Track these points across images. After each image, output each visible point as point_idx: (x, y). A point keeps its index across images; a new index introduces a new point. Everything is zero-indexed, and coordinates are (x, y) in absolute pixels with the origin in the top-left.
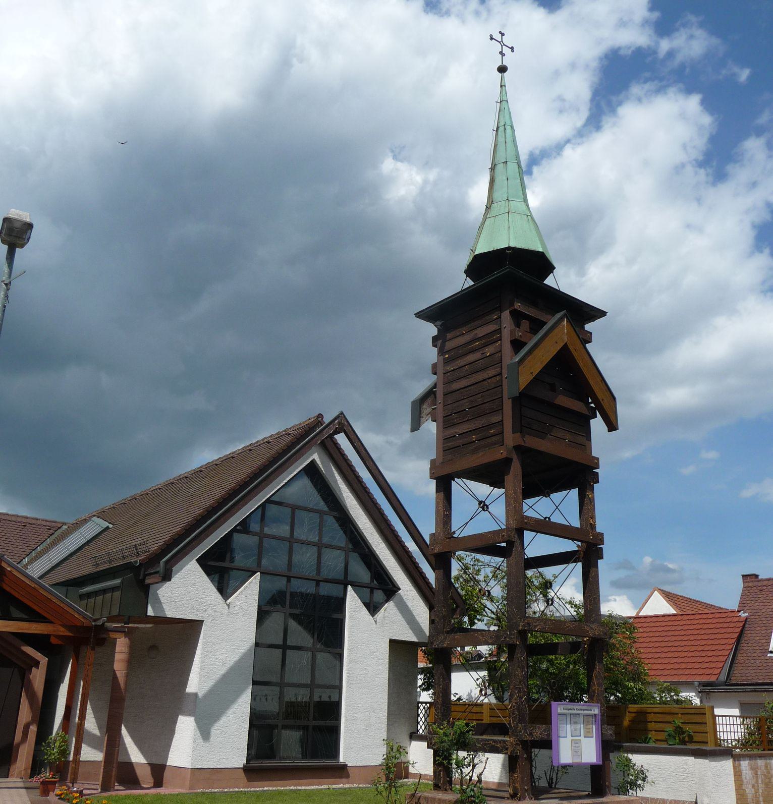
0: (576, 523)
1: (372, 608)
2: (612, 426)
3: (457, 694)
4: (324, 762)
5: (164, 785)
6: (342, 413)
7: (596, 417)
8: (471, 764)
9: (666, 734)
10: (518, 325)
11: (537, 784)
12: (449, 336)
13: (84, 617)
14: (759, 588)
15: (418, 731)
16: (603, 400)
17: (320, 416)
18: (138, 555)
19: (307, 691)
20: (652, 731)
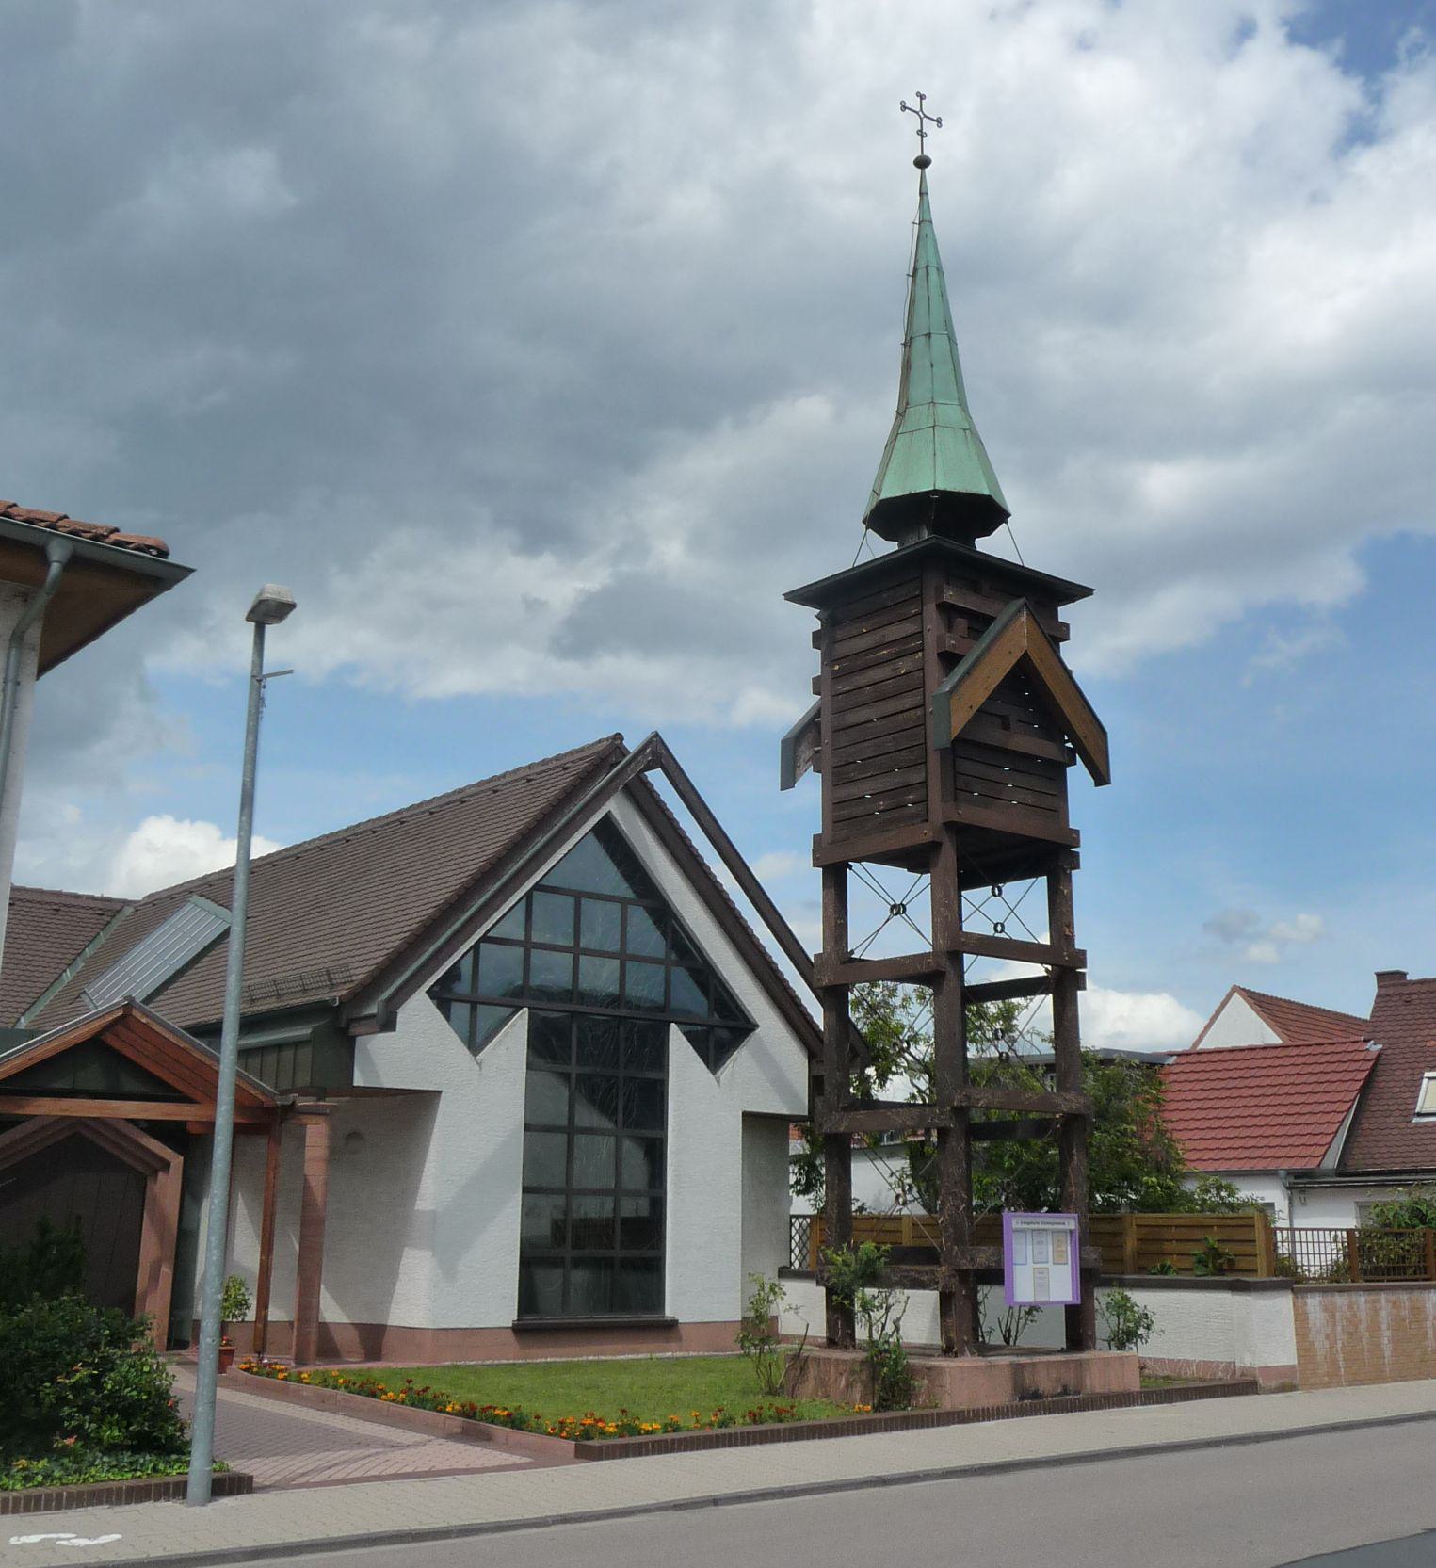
0: (1045, 939)
1: (712, 1058)
2: (1101, 777)
6: (657, 735)
7: (1075, 764)
8: (885, 1306)
9: (1194, 1259)
10: (950, 627)
11: (987, 1339)
12: (840, 634)
13: (263, 1094)
15: (791, 1264)
16: (1085, 737)
18: (332, 986)
19: (609, 1203)
20: (1172, 1254)
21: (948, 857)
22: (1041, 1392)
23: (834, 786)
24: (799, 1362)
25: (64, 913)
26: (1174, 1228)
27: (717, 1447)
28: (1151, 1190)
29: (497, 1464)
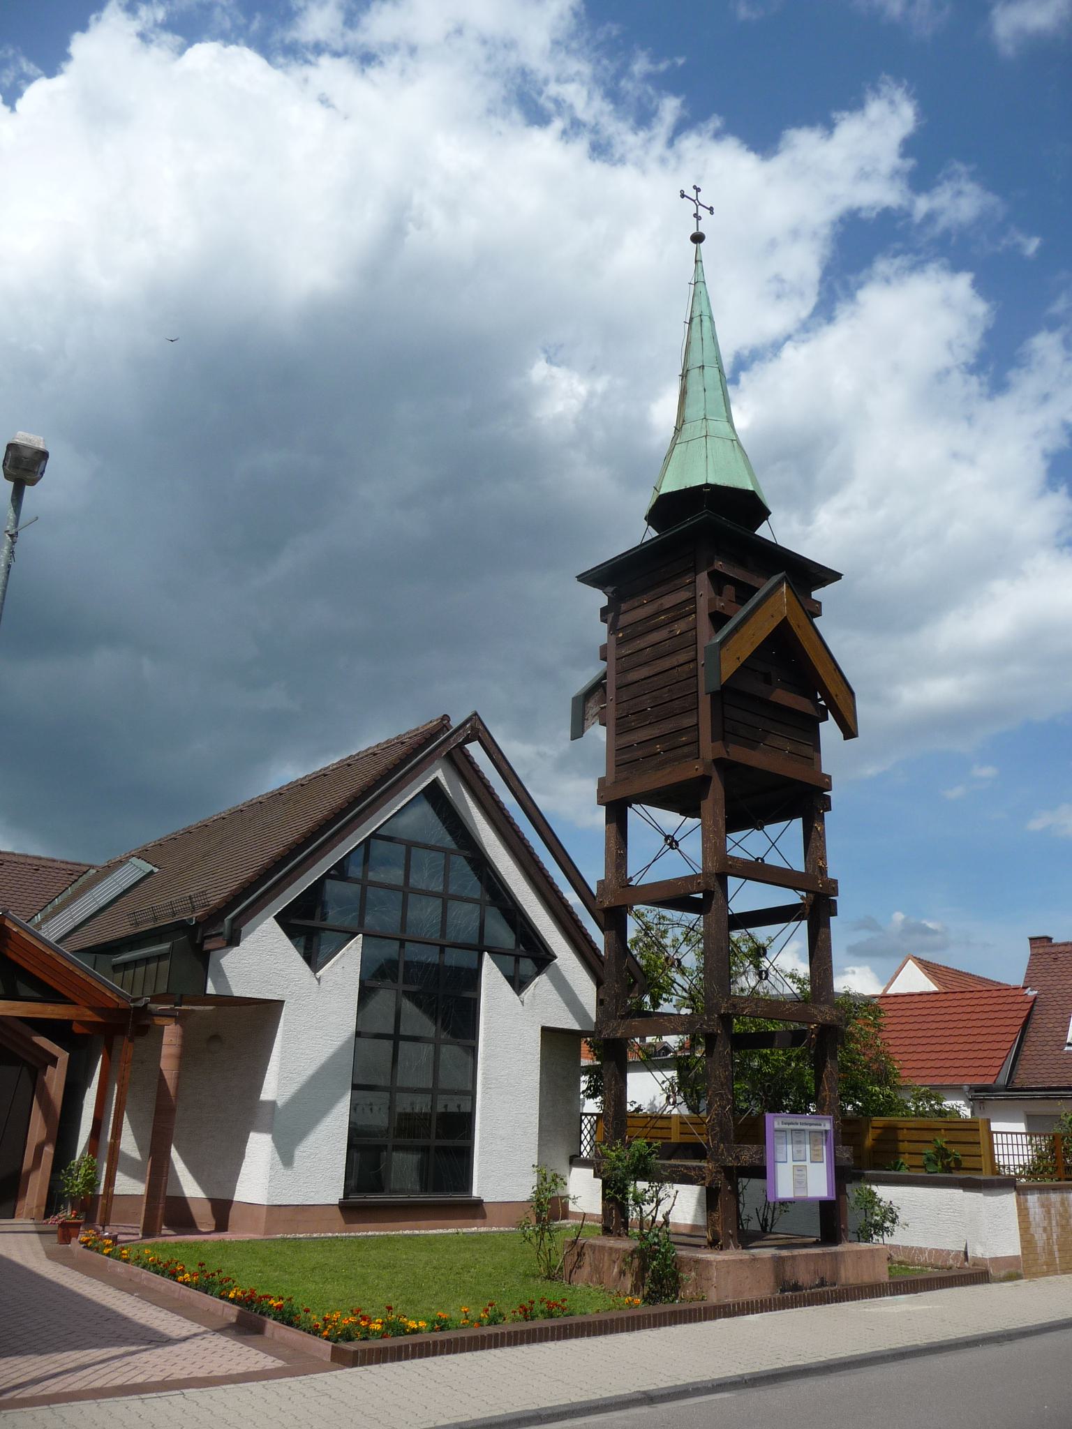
0: (799, 865)
1: (517, 984)
2: (849, 731)
3: (635, 1103)
4: (450, 1197)
5: (229, 1228)
6: (476, 714)
8: (655, 1199)
10: (719, 592)
11: (745, 1226)
12: (624, 607)
13: (119, 997)
14: (1053, 956)
15: (581, 1153)
17: (446, 717)
18: (194, 910)
20: (904, 1153)
21: (716, 790)
22: (800, 1284)
23: (617, 735)
24: (578, 1250)
25: (41, 872)
26: (905, 1130)
27: (483, 1348)
28: (874, 1098)
29: (241, 1369)
